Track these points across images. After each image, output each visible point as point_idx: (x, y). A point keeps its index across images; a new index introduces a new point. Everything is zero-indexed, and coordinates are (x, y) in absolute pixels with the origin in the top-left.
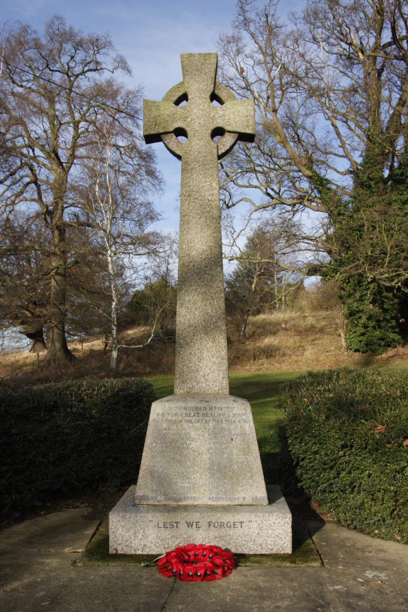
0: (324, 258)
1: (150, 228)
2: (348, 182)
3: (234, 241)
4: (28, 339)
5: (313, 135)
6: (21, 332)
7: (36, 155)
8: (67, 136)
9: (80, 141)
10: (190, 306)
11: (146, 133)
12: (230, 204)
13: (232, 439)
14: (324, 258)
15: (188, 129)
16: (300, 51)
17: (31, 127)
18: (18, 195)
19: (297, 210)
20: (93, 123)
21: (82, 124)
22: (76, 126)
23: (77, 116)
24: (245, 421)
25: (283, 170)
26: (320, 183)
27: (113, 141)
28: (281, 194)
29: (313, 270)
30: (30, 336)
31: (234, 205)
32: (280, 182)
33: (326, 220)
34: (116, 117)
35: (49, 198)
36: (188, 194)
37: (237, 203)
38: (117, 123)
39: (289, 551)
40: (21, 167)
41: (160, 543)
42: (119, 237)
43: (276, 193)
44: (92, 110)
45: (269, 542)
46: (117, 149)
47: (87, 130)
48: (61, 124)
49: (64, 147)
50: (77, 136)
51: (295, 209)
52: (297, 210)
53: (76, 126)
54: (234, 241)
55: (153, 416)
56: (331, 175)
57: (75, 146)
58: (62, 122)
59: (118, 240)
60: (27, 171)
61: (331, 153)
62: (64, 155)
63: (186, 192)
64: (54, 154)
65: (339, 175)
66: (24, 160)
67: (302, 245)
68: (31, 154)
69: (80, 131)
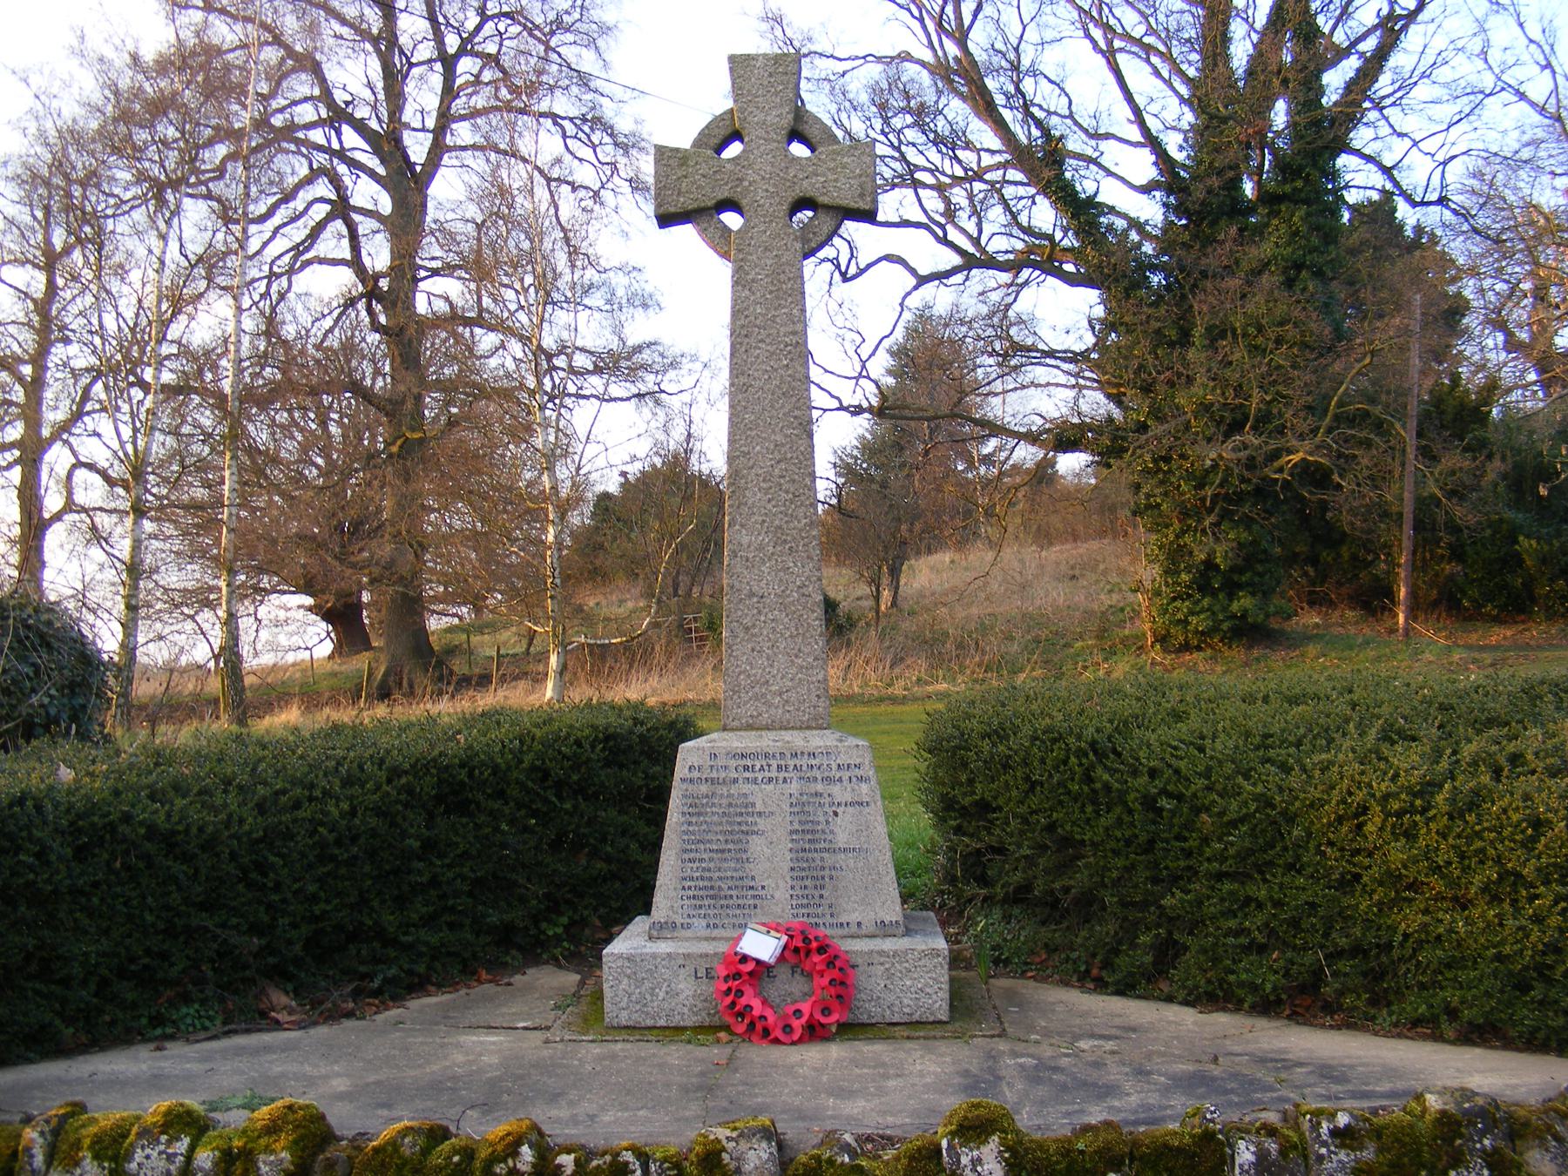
0: (1095, 404)
1: (639, 329)
2: (1151, 210)
3: (864, 367)
4: (323, 625)
5: (1062, 89)
6: (310, 609)
7: (347, 146)
8: (423, 95)
9: (459, 105)
10: (751, 555)
11: (661, 211)
12: (852, 270)
13: (836, 814)
14: (1095, 404)
15: (744, 202)
16: (939, 130)
17: (332, 74)
18: (298, 249)
19: (1026, 283)
20: (493, 60)
21: (466, 66)
22: (449, 63)
23: (452, 42)
24: (861, 779)
25: (986, 182)
26: (1082, 212)
27: (544, 106)
28: (983, 243)
29: (1065, 437)
30: (328, 616)
31: (861, 272)
32: (977, 214)
33: (1099, 312)
34: (553, 44)
35: (378, 255)
36: (744, 332)
37: (869, 266)
38: (554, 57)
39: (943, 1016)
40: (308, 181)
41: (700, 1005)
42: (560, 353)
43: (969, 236)
44: (489, 28)
45: (906, 1001)
46: (555, 123)
47: (477, 77)
48: (411, 65)
49: (419, 126)
50: (449, 92)
51: (1020, 281)
52: (1026, 283)
53: (449, 63)
54: (864, 367)
55: (680, 770)
56: (1110, 193)
57: (445, 119)
58: (414, 60)
59: (561, 362)
60: (323, 188)
61: (1108, 136)
62: (417, 148)
63: (743, 326)
64: (388, 144)
65: (1127, 190)
66: (321, 159)
67: (1040, 373)
68: (335, 145)
69: (459, 82)
